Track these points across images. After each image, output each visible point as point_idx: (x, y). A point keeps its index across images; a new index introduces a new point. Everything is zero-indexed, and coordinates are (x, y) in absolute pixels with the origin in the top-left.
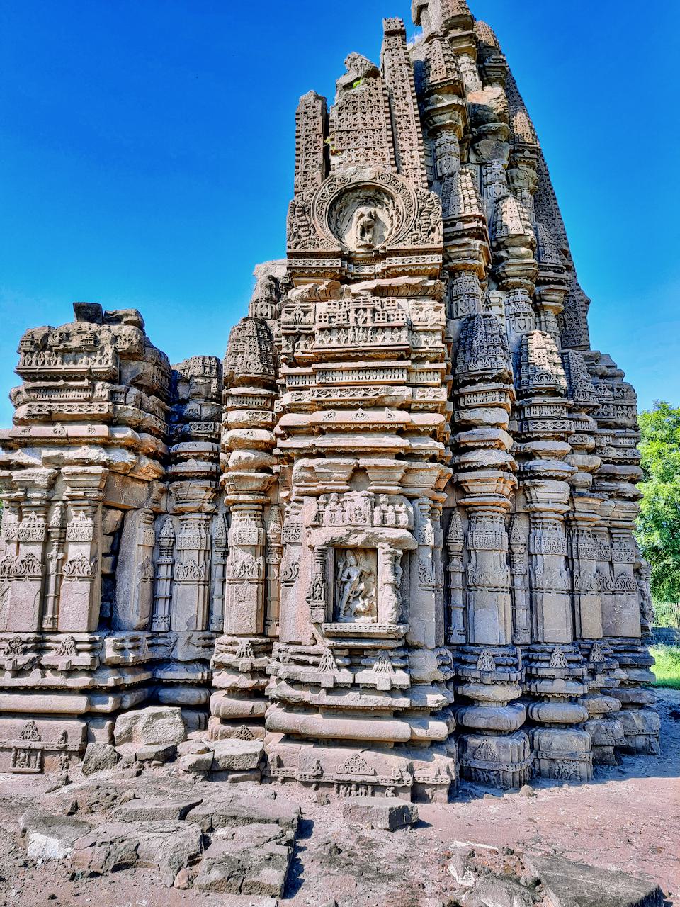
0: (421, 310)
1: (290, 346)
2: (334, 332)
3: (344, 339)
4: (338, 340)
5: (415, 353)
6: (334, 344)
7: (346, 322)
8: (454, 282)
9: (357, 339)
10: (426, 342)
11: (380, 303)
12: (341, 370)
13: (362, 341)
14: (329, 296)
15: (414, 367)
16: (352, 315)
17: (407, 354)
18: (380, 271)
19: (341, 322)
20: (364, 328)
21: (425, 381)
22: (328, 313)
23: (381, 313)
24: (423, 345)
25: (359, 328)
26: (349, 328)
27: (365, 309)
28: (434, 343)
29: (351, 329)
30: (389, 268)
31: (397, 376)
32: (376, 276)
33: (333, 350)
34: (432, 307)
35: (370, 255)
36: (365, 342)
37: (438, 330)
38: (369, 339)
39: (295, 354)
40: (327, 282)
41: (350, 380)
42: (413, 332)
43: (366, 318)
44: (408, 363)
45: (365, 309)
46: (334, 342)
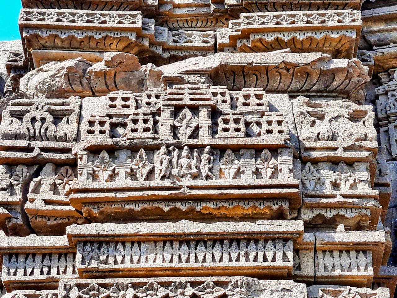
0: (321, 118)
1: (17, 189)
2: (122, 155)
3: (145, 172)
4: (132, 175)
5: (312, 207)
6: (122, 181)
7: (149, 134)
8: (380, 90)
9: (175, 172)
10: (335, 185)
11: (227, 98)
12: (137, 241)
13: (189, 175)
14: (111, 85)
15: (309, 237)
16: (165, 120)
17: (292, 209)
18: (227, 41)
19: (141, 134)
20: (192, 148)
21: (337, 272)
22: (110, 116)
23: (231, 117)
24: (328, 190)
25: (180, 148)
26: (158, 147)
27: (195, 110)
28: (353, 186)
29: (163, 149)
30: (246, 34)
31: (270, 255)
32: (216, 49)
33: (119, 195)
34: (344, 112)
35: (203, 10)
36: (195, 177)
37: (361, 160)
38: (205, 171)
39: (28, 205)
40: (108, 56)
41: (159, 264)
42: (304, 162)
43: (197, 128)
44: (298, 226)
45: (195, 110)
46: (121, 178)
